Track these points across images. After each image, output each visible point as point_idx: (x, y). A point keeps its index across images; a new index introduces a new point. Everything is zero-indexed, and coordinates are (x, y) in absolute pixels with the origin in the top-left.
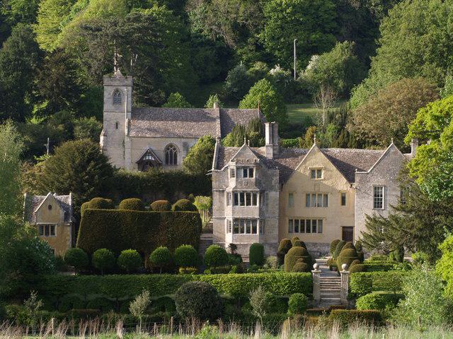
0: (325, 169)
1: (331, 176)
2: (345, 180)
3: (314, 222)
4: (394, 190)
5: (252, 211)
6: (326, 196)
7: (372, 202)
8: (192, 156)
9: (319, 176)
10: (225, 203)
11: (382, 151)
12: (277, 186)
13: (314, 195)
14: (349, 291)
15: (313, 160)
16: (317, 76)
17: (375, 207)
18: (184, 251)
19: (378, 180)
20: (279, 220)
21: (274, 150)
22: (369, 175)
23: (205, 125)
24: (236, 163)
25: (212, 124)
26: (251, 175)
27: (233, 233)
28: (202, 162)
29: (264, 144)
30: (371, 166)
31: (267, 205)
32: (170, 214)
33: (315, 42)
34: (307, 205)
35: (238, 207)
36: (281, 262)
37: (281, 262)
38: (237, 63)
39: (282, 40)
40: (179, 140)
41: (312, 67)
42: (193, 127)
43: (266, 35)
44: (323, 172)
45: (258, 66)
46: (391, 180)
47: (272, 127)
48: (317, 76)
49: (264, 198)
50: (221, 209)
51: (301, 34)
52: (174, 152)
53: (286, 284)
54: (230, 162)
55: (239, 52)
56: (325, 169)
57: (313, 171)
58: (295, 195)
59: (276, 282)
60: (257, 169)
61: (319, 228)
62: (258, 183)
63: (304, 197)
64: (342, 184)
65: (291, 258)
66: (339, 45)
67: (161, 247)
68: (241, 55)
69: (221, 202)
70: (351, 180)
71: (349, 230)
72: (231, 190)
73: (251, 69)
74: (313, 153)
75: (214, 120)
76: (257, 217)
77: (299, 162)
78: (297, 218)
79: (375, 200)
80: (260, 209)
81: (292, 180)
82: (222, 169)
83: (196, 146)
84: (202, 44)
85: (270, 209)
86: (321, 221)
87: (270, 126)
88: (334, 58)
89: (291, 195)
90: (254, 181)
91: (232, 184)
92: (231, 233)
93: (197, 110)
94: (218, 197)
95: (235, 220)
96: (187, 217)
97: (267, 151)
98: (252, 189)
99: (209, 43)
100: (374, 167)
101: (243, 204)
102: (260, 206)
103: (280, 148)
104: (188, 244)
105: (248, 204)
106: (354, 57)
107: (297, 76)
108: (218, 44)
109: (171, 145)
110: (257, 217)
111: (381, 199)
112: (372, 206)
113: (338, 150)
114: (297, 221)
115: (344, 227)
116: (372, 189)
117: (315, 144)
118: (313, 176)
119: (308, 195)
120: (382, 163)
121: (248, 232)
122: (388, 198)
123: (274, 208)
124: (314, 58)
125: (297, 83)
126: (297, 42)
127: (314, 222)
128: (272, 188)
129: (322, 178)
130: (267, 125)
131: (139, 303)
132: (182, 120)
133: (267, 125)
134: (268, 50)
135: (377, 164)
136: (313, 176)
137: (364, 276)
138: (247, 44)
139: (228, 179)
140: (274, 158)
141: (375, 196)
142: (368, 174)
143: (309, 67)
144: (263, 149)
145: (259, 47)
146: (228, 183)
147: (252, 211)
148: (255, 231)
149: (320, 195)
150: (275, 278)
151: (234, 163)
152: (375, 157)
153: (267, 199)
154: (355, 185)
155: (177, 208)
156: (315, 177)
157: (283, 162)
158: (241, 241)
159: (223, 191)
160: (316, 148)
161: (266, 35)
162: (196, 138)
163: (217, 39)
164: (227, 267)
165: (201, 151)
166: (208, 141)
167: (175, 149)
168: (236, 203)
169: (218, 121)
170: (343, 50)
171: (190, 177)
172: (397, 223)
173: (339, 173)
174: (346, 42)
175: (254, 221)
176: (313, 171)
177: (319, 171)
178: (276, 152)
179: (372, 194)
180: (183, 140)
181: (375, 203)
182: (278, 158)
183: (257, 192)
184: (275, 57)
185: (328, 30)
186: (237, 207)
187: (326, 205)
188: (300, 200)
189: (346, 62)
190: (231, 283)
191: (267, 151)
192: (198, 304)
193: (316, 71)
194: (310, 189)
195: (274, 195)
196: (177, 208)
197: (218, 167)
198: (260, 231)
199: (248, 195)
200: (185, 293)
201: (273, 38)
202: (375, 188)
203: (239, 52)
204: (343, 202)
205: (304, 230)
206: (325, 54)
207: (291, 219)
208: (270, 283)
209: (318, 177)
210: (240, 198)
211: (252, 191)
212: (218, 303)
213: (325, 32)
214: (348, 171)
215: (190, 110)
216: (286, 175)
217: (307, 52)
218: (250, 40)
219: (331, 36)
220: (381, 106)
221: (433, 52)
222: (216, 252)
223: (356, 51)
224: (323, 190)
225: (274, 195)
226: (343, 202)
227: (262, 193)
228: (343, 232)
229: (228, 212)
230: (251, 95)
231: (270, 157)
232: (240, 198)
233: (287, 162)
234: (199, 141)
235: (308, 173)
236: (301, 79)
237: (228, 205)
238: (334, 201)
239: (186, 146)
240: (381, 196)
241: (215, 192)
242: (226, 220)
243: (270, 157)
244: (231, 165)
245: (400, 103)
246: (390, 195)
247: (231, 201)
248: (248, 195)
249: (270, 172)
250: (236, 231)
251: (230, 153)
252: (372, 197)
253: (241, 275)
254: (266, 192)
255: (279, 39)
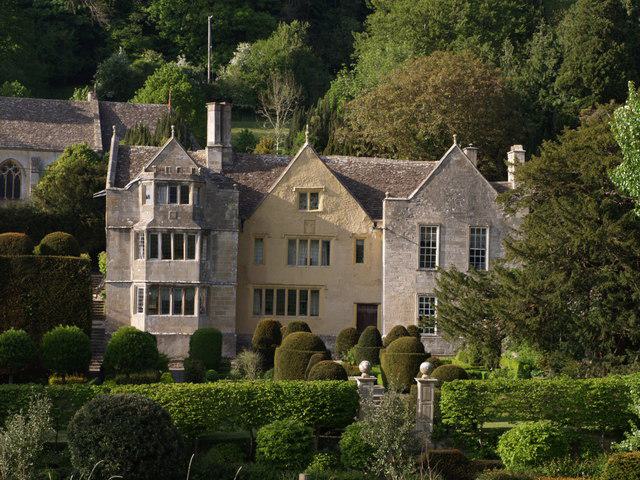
0: (326, 191)
1: (337, 205)
2: (364, 214)
3: (304, 293)
4: (459, 233)
5: (187, 270)
6: (327, 244)
7: (416, 256)
8: (50, 180)
9: (315, 205)
10: (132, 254)
11: (427, 164)
12: (235, 222)
13: (303, 242)
14: (437, 421)
15: (303, 174)
16: (249, 76)
17: (422, 265)
18: (64, 338)
19: (427, 215)
20: (238, 287)
21: (223, 156)
22: (411, 205)
23: (72, 129)
24: (156, 175)
25: (85, 128)
26: (185, 200)
27: (147, 314)
28: (72, 190)
29: (203, 144)
30: (414, 188)
31: (215, 258)
32: (31, 262)
33: (241, 23)
34: (290, 261)
35: (159, 261)
36: (266, 364)
37: (266, 364)
38: (115, 49)
39: (188, 17)
40: (24, 152)
41: (239, 62)
42: (50, 132)
43: (160, 7)
44: (321, 198)
45: (148, 57)
46: (451, 213)
47: (220, 111)
48: (249, 76)
49: (208, 243)
50: (123, 266)
51: (220, 10)
52: (15, 175)
53: (305, 406)
54: (143, 172)
55: (114, 34)
56: (326, 191)
57: (302, 195)
58: (267, 241)
59: (281, 402)
60: (195, 187)
61: (312, 309)
62: (197, 215)
63: (285, 245)
64: (357, 221)
65: (289, 356)
66: (283, 28)
67: (12, 331)
68: (118, 40)
69: (124, 252)
70: (375, 214)
71: (370, 311)
72: (144, 228)
73: (137, 62)
74: (303, 159)
75: (90, 121)
76: (195, 281)
77: (277, 176)
78: (270, 287)
79: (422, 251)
80: (202, 265)
81: (262, 212)
82: (127, 187)
83: (58, 163)
84: (52, 18)
85: (219, 266)
86: (315, 293)
87: (216, 110)
88: (276, 48)
89: (260, 240)
90: (190, 210)
91: (145, 216)
92: (143, 313)
93: (57, 102)
94: (117, 239)
95: (152, 287)
96: (67, 269)
97: (209, 158)
98: (187, 225)
99: (65, 17)
100: (421, 189)
101: (166, 255)
102: (201, 260)
103: (234, 154)
104: (70, 324)
105: (179, 255)
106: (308, 49)
107: (214, 76)
108: (81, 20)
109: (9, 163)
110: (195, 281)
111: (434, 251)
112: (416, 264)
113: (345, 159)
114: (269, 292)
115: (360, 305)
116: (417, 231)
117: (306, 144)
118: (302, 206)
119: (292, 243)
120: (435, 182)
121: (177, 310)
122: (447, 248)
123: (228, 266)
124: (243, 47)
125: (213, 88)
126: (212, 21)
127: (304, 293)
128: (225, 226)
129: (320, 209)
130: (211, 109)
131: (95, 368)
132: (31, 119)
133: (211, 109)
134: (163, 34)
135: (427, 183)
136: (302, 206)
137: (471, 388)
138: (129, 22)
139: (138, 207)
140: (224, 171)
141: (422, 244)
142: (409, 201)
143: (234, 62)
144: (204, 154)
145: (149, 28)
146: (138, 213)
147: (187, 270)
148: (190, 310)
149: (315, 242)
150: (279, 392)
151: (151, 175)
152: (415, 174)
153: (216, 248)
154: (384, 222)
155: (45, 249)
156: (305, 207)
157: (241, 179)
158: (162, 328)
159: (128, 230)
160: (310, 151)
161: (160, 7)
162: (57, 151)
163: (79, 12)
164: (151, 375)
165: (68, 170)
166: (82, 153)
167: (16, 170)
168: (153, 254)
169: (98, 123)
170: (292, 36)
171: (47, 217)
172: (516, 283)
173: (352, 199)
174: (295, 22)
175: (189, 289)
176: (302, 195)
177: (315, 195)
178: (227, 160)
179: (417, 240)
180: (33, 154)
181: (422, 258)
182: (231, 172)
183: (196, 232)
184: (175, 45)
185: (262, 5)
186: (156, 261)
187: (327, 261)
188: (276, 250)
189: (296, 55)
190: (182, 405)
191: (209, 158)
192: (127, 447)
193: (245, 68)
194: (297, 230)
195: (228, 239)
196: (45, 249)
197: (118, 182)
198: (200, 313)
199: (179, 238)
200: (96, 422)
201: (171, 14)
202: (423, 230)
203: (114, 34)
204: (359, 258)
205: (283, 310)
206: (259, 43)
207: (258, 287)
208: (268, 404)
209: (311, 208)
210: (161, 244)
211: (186, 231)
212: (175, 444)
213: (257, 9)
214: (369, 199)
215: (44, 102)
216: (250, 202)
217: (227, 41)
218: (133, 16)
219: (267, 16)
220: (398, 95)
221: (471, 17)
222: (133, 340)
223: (312, 37)
224: (321, 232)
225: (228, 239)
226: (359, 258)
227: (205, 233)
228: (359, 314)
229: (139, 273)
230: (148, 88)
231: (217, 168)
232: (161, 244)
233: (252, 179)
234: (65, 154)
235: (293, 198)
236: (221, 81)
237: (137, 256)
238: (341, 253)
239: (39, 168)
240: (434, 245)
241: (112, 232)
242: (132, 289)
243: (217, 168)
244: (146, 179)
245: (436, 89)
246: (451, 244)
247: (143, 251)
248: (179, 238)
249: (221, 193)
250: (151, 311)
251: (140, 157)
252: (416, 247)
253: (202, 386)
254: (212, 233)
255: (181, 15)
